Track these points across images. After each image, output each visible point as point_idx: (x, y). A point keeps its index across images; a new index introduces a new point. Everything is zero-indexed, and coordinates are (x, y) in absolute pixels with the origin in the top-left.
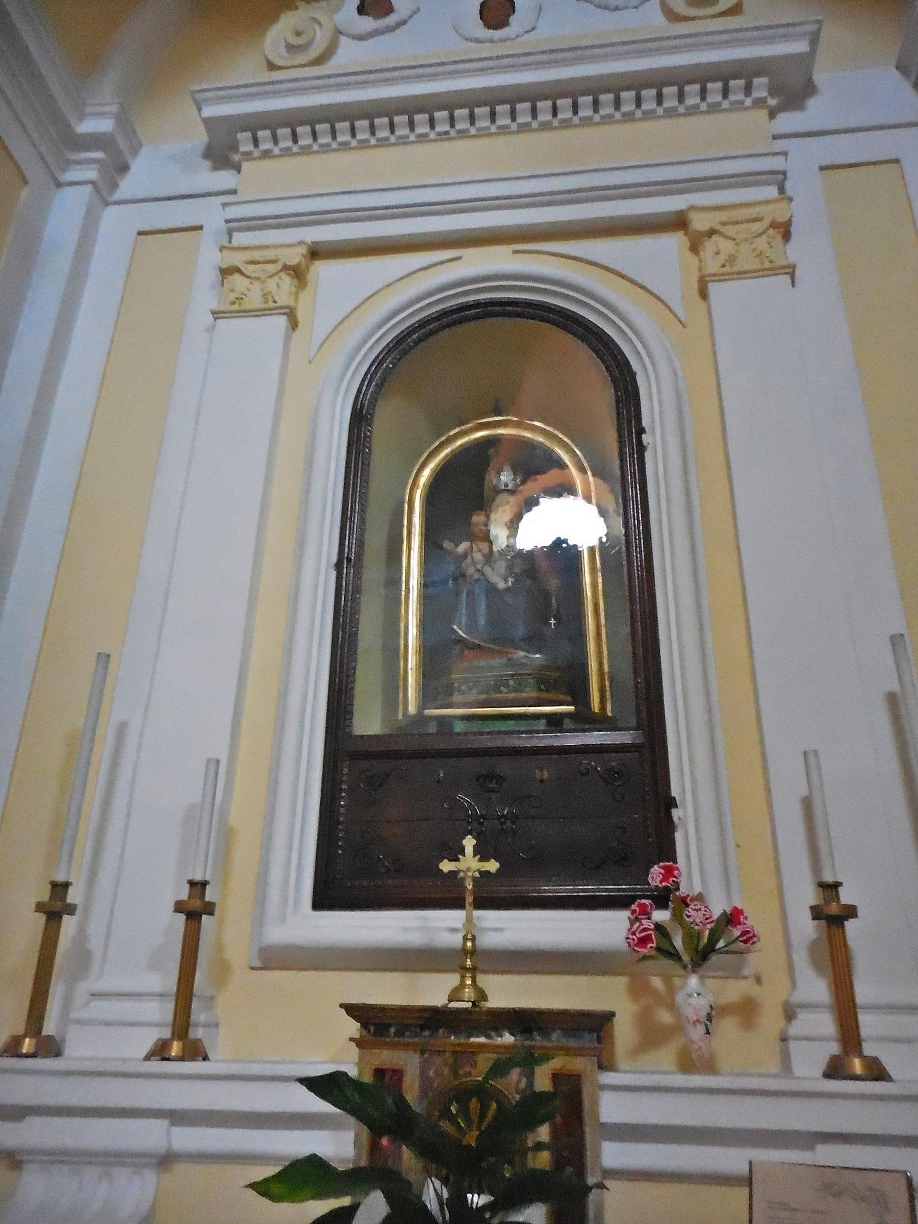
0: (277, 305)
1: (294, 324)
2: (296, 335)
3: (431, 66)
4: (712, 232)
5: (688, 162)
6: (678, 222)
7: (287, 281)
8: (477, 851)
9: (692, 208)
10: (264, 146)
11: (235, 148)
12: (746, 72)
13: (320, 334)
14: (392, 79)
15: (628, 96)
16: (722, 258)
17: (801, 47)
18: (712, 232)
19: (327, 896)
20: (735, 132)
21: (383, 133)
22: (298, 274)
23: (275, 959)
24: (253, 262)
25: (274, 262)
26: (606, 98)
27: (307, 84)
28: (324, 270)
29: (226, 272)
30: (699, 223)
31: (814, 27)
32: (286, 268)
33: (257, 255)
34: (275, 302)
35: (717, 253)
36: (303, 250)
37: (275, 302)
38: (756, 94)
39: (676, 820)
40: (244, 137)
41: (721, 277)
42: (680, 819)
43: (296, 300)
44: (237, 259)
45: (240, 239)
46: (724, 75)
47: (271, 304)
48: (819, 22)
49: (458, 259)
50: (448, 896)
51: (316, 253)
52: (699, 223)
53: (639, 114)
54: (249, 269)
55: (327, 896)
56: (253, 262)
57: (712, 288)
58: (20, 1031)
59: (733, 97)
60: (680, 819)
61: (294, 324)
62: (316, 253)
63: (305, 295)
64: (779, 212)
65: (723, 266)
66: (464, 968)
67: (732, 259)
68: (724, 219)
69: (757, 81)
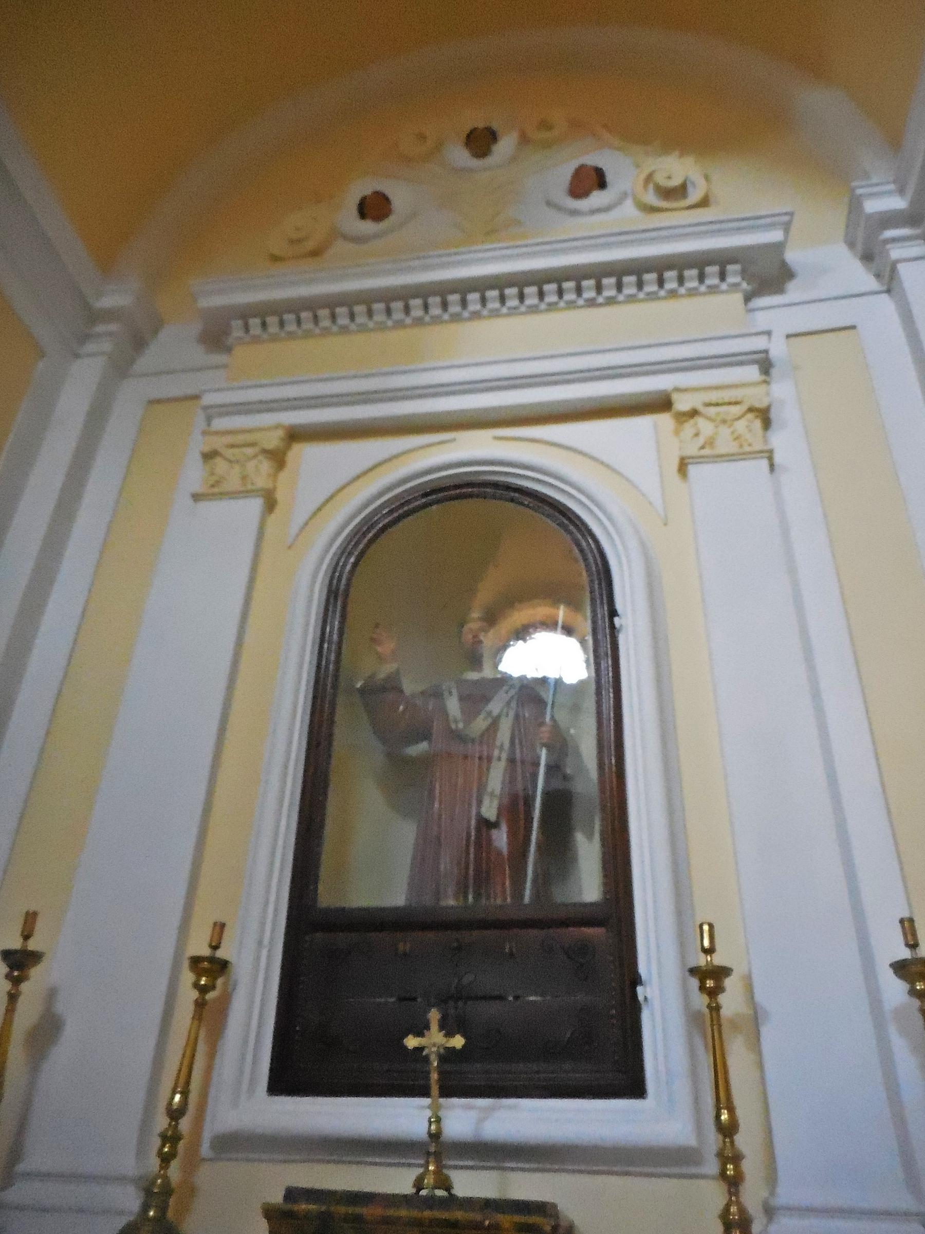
0: (254, 487)
1: (270, 504)
2: (272, 519)
3: (684, 226)
4: (694, 413)
5: (609, 350)
6: (661, 403)
7: (266, 466)
8: (419, 1034)
9: (677, 390)
10: (612, 293)
11: (227, 332)
12: (722, 261)
13: (300, 516)
14: (758, 227)
15: (397, 305)
16: (701, 440)
17: (775, 236)
18: (694, 413)
19: (286, 1079)
20: (713, 315)
21: (326, 323)
22: (278, 458)
23: (233, 1144)
24: (232, 446)
25: (252, 445)
26: (651, 277)
27: (681, 231)
28: (309, 454)
29: (209, 456)
30: (682, 404)
31: (786, 218)
32: (265, 451)
33: (240, 439)
34: (252, 484)
35: (697, 435)
36: (280, 433)
37: (252, 484)
38: (731, 280)
39: (641, 998)
40: (237, 324)
41: (700, 460)
42: (646, 998)
43: (275, 481)
44: (218, 443)
45: (220, 423)
46: (699, 263)
47: (249, 487)
48: (791, 214)
49: (454, 440)
50: (405, 1080)
51: (295, 435)
52: (682, 404)
53: (427, 319)
54: (229, 453)
55: (286, 1079)
56: (232, 446)
57: (692, 470)
58: (454, 1192)
59: (709, 282)
60: (646, 998)
61: (270, 504)
62: (295, 435)
63: (283, 476)
64: (757, 396)
65: (703, 447)
66: (428, 1154)
67: (710, 442)
68: (707, 400)
69: (730, 268)
